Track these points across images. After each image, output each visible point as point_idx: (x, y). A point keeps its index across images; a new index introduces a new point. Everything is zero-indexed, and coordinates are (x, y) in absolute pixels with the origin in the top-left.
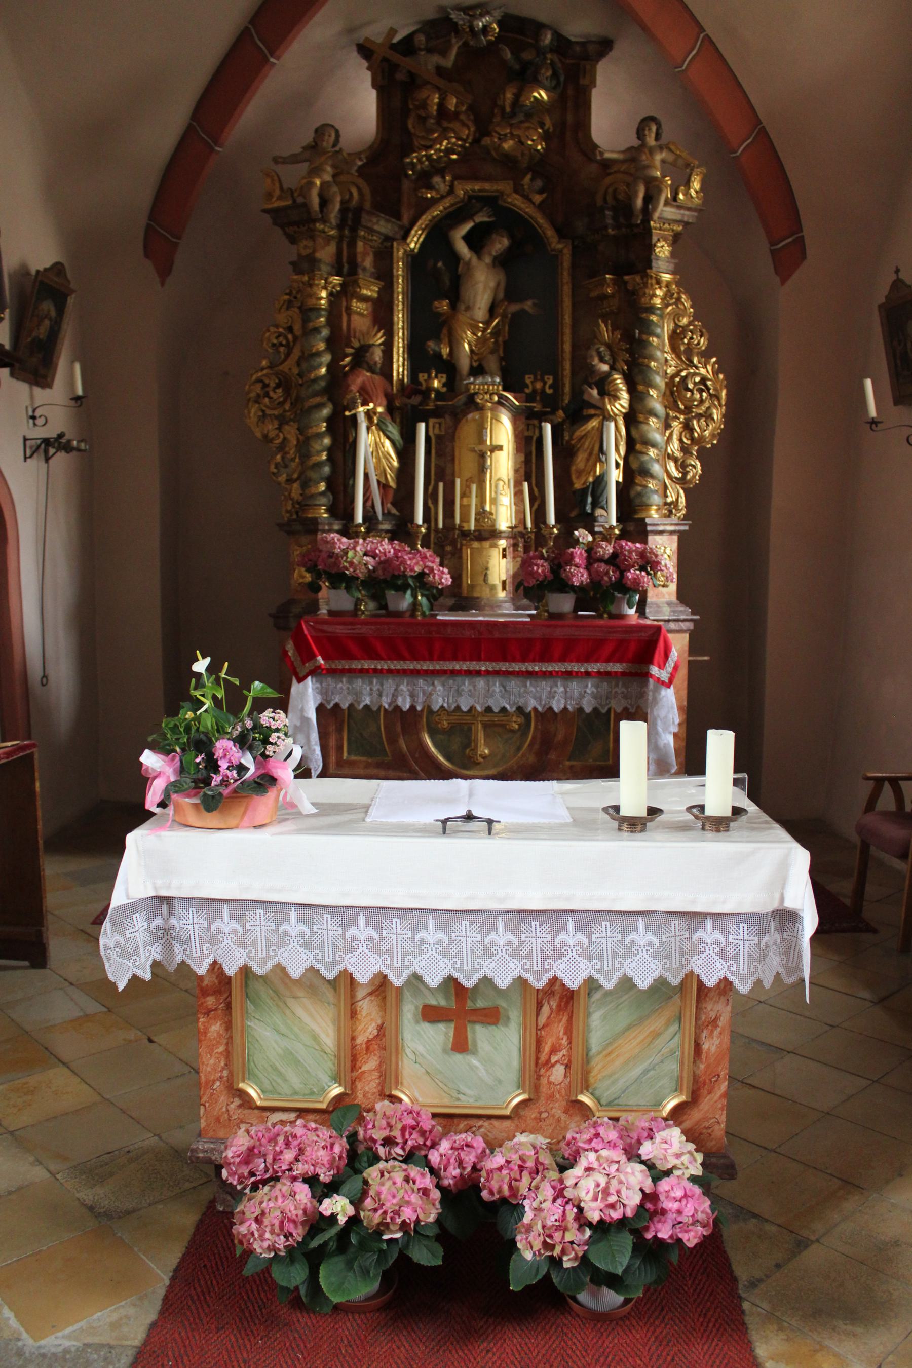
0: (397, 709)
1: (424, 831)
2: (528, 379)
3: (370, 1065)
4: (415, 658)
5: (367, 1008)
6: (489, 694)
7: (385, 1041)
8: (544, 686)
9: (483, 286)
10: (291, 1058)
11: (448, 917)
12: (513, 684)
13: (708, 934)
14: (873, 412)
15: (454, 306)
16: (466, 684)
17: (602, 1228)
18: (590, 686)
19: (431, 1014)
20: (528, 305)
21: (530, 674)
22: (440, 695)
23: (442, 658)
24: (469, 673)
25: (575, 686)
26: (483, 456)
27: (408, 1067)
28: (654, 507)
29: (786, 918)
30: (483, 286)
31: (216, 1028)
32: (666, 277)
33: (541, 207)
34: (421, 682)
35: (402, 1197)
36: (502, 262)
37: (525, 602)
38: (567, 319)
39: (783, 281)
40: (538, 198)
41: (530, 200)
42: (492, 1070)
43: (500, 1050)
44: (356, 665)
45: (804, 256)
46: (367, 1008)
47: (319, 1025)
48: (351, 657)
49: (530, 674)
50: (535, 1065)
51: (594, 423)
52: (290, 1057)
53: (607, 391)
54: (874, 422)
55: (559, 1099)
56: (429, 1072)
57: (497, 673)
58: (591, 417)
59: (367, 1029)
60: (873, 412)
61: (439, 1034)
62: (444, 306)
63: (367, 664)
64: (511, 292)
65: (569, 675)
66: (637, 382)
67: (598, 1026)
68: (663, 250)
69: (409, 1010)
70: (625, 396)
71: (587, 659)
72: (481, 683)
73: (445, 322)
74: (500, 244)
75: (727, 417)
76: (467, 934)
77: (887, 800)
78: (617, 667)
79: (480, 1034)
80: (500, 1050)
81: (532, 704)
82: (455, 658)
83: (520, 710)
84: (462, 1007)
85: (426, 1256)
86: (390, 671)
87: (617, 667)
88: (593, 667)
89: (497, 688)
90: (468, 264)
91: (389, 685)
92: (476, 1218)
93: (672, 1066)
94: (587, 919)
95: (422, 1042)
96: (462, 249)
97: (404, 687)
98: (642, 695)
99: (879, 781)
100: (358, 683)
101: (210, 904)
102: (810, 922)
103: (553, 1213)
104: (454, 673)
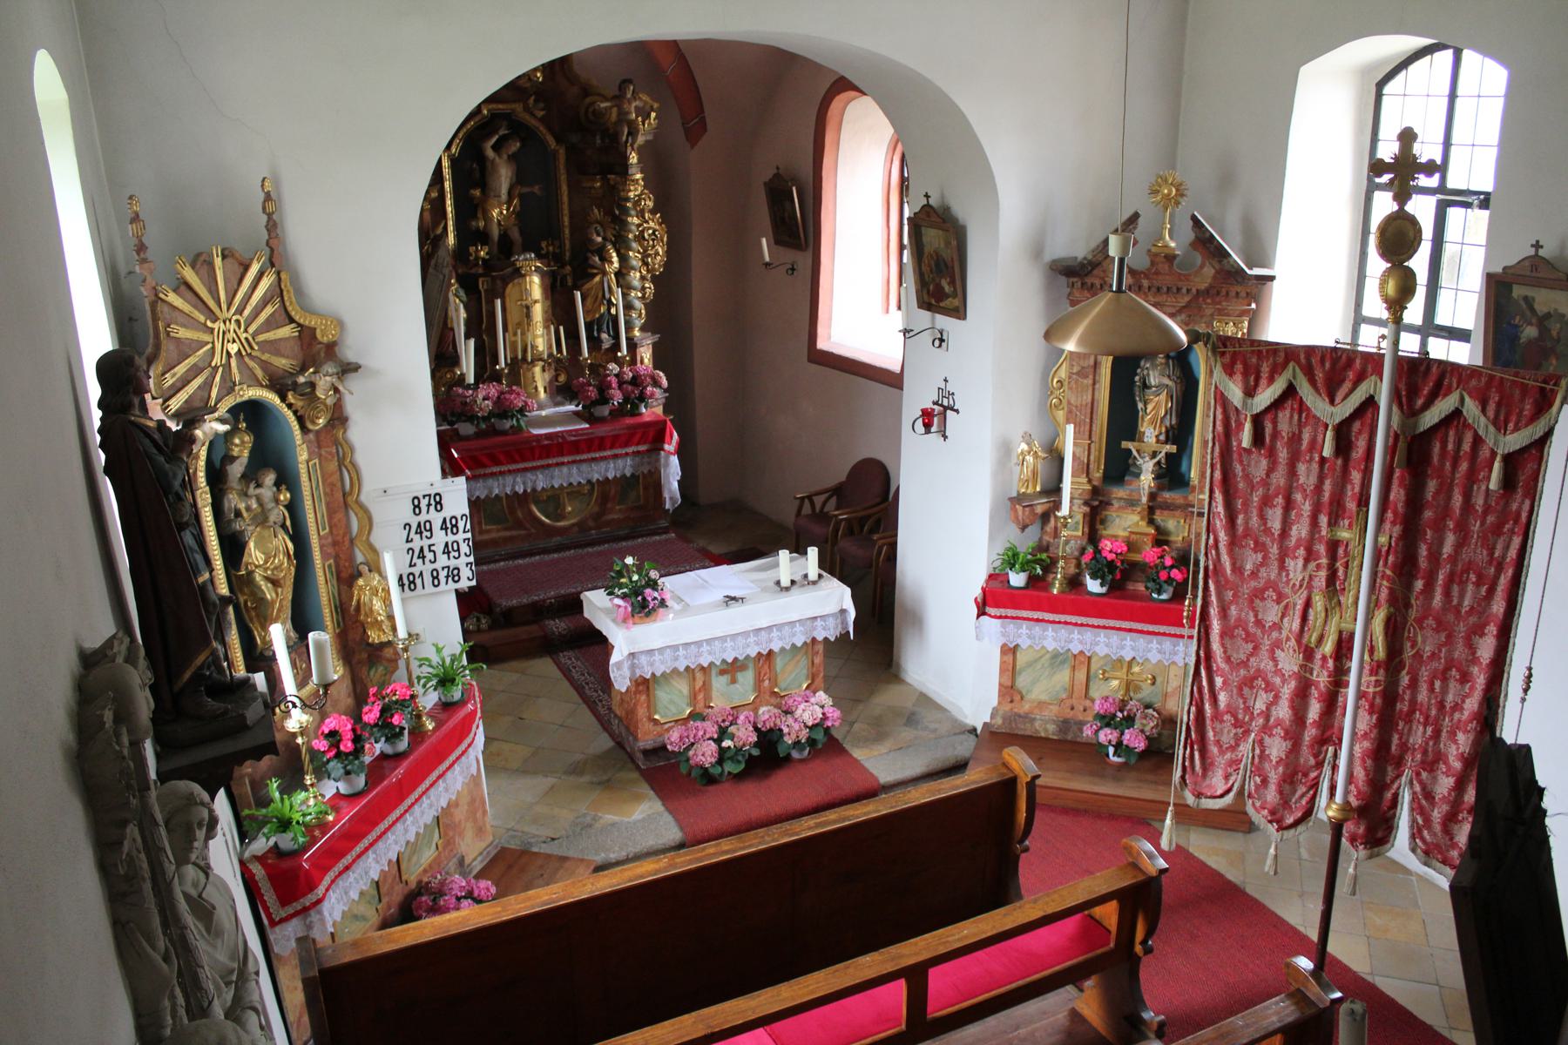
0: (516, 493)
1: (714, 606)
2: (544, 244)
3: (700, 697)
4: (524, 460)
5: (699, 675)
6: (570, 474)
7: (706, 687)
8: (603, 465)
9: (504, 176)
10: (672, 703)
11: (734, 637)
12: (584, 467)
13: (819, 623)
14: (767, 259)
15: (483, 192)
16: (556, 471)
17: (815, 726)
18: (629, 461)
19: (722, 672)
20: (536, 189)
21: (594, 459)
22: (541, 481)
23: (540, 458)
24: (557, 464)
25: (620, 462)
26: (528, 308)
27: (715, 694)
28: (1111, 750)
29: (843, 611)
30: (504, 176)
31: (643, 698)
32: (638, 176)
33: (541, 120)
34: (529, 475)
35: (744, 735)
36: (512, 158)
37: (559, 399)
38: (565, 199)
39: (693, 144)
40: (541, 114)
41: (533, 115)
42: (744, 689)
43: (747, 678)
44: (488, 471)
45: (705, 130)
46: (699, 675)
47: (683, 687)
48: (484, 466)
49: (594, 459)
50: (759, 681)
51: (597, 279)
52: (672, 702)
53: (605, 259)
54: (767, 264)
55: (768, 690)
56: (724, 694)
57: (574, 462)
58: (594, 275)
59: (699, 684)
60: (767, 259)
61: (725, 679)
62: (477, 193)
63: (495, 469)
64: (519, 179)
65: (616, 456)
66: (621, 245)
67: (779, 663)
68: (634, 158)
69: (714, 672)
70: (615, 259)
71: (626, 445)
72: (565, 469)
73: (476, 206)
74: (515, 146)
75: (668, 253)
76: (741, 641)
77: (807, 509)
78: (642, 448)
79: (739, 676)
80: (747, 678)
81: (596, 477)
82: (548, 457)
83: (589, 482)
84: (732, 669)
85: (755, 752)
86: (509, 471)
87: (642, 448)
88: (630, 450)
89: (574, 470)
90: (493, 161)
91: (509, 479)
92: (768, 739)
93: (805, 671)
94: (780, 627)
95: (719, 683)
96: (490, 153)
97: (518, 479)
98: (658, 460)
99: (802, 499)
100: (490, 482)
101: (650, 652)
102: (852, 614)
103: (796, 727)
104: (549, 466)
